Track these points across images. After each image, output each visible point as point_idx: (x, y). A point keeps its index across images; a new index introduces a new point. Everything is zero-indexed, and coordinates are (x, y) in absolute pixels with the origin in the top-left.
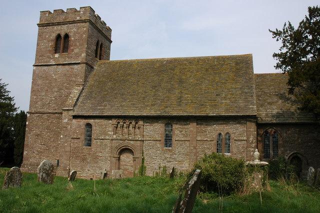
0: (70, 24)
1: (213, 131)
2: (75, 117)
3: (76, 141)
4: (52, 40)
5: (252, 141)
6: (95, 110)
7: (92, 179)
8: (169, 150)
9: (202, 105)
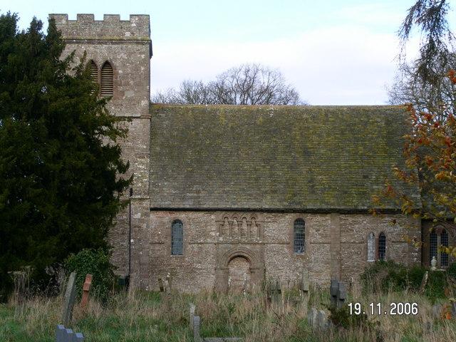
6: (183, 199)
8: (302, 257)
9: (346, 193)
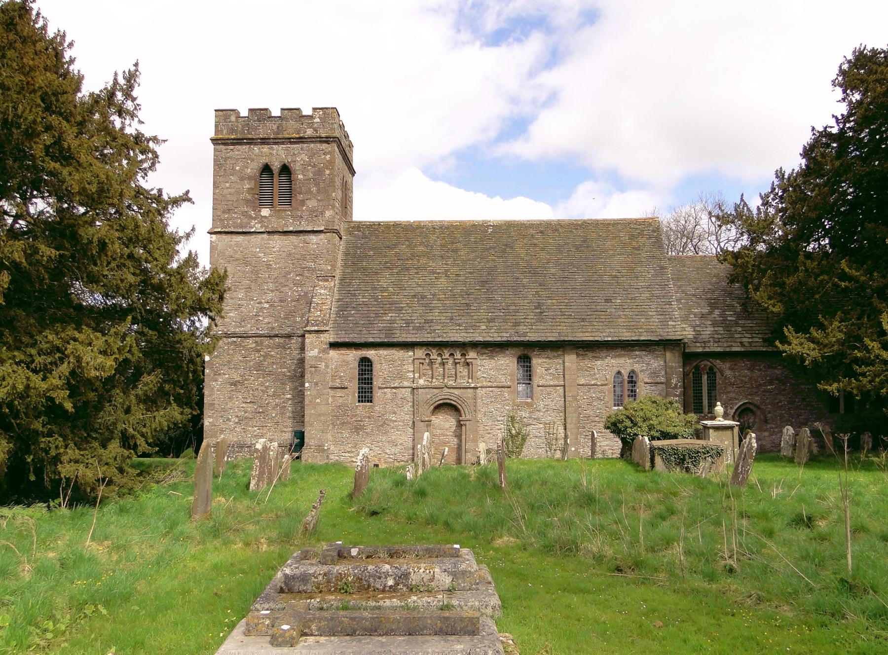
0: (291, 143)
1: (608, 367)
2: (334, 345)
3: (339, 393)
4: (250, 178)
5: (676, 385)
7: (377, 466)
